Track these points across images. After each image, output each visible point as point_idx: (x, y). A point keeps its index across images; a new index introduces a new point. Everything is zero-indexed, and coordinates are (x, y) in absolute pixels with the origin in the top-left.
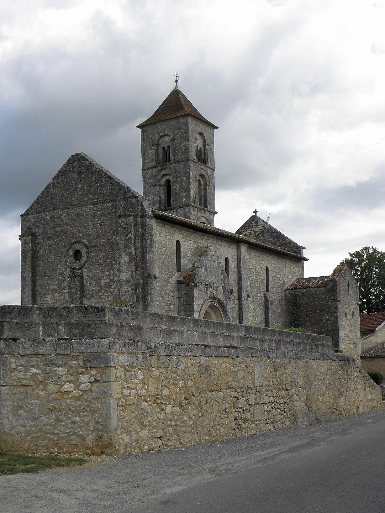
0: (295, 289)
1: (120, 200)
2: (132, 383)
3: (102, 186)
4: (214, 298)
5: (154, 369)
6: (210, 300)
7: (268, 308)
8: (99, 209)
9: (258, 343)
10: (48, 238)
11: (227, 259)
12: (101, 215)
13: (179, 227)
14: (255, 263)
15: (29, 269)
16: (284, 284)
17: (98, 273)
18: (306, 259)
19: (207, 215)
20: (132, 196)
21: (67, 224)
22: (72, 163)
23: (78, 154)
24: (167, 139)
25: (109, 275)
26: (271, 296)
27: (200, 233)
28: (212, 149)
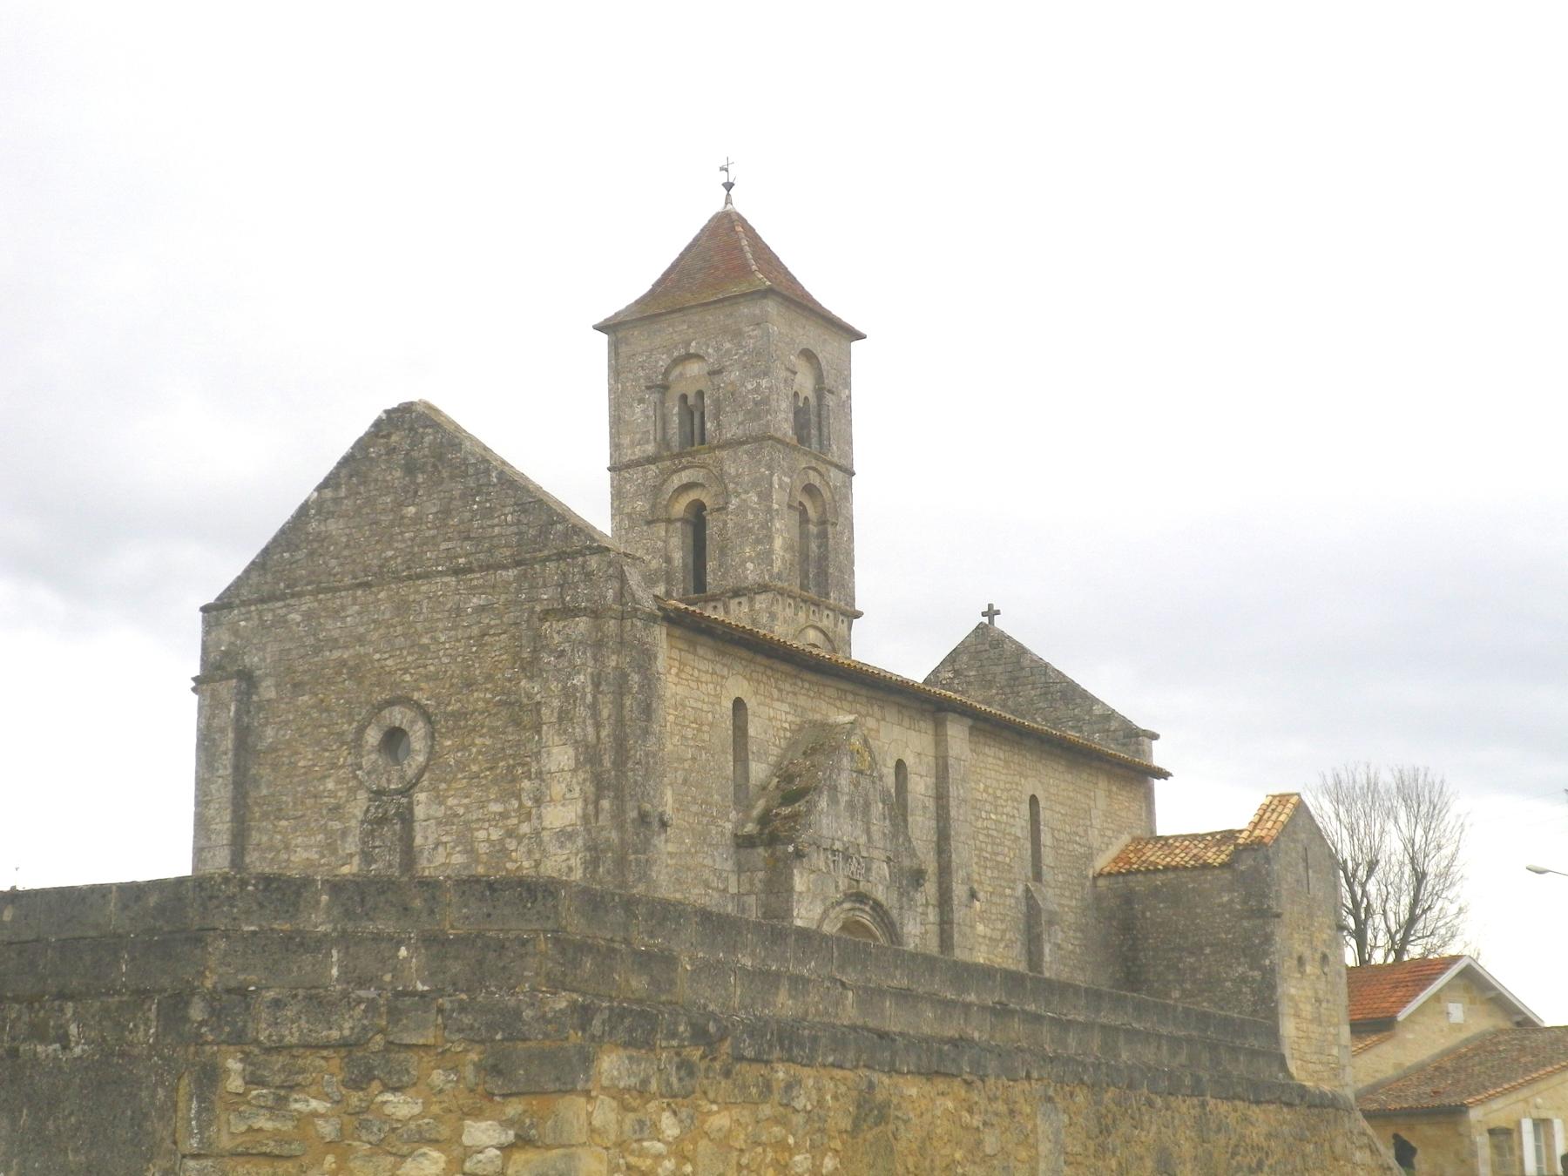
0: (1129, 872)
1: (548, 559)
2: (642, 1153)
3: (488, 513)
4: (861, 898)
5: (715, 1108)
6: (847, 905)
7: (1039, 936)
8: (473, 590)
9: (1046, 1034)
10: (295, 686)
11: (900, 765)
12: (481, 609)
13: (744, 653)
14: (993, 785)
15: (222, 792)
16: (1089, 857)
17: (466, 807)
18: (1163, 774)
19: (826, 623)
20: (589, 548)
21: (361, 640)
22: (388, 436)
23: (406, 408)
24: (694, 368)
25: (504, 815)
26: (1050, 898)
27: (814, 678)
28: (845, 407)
